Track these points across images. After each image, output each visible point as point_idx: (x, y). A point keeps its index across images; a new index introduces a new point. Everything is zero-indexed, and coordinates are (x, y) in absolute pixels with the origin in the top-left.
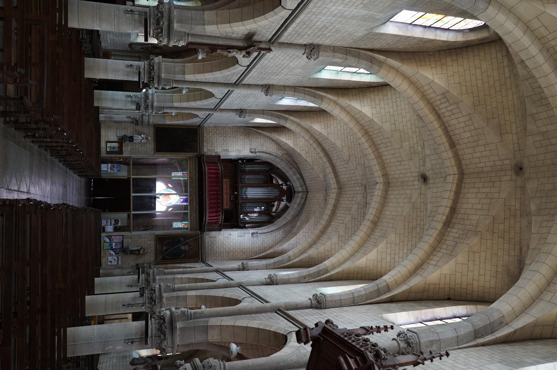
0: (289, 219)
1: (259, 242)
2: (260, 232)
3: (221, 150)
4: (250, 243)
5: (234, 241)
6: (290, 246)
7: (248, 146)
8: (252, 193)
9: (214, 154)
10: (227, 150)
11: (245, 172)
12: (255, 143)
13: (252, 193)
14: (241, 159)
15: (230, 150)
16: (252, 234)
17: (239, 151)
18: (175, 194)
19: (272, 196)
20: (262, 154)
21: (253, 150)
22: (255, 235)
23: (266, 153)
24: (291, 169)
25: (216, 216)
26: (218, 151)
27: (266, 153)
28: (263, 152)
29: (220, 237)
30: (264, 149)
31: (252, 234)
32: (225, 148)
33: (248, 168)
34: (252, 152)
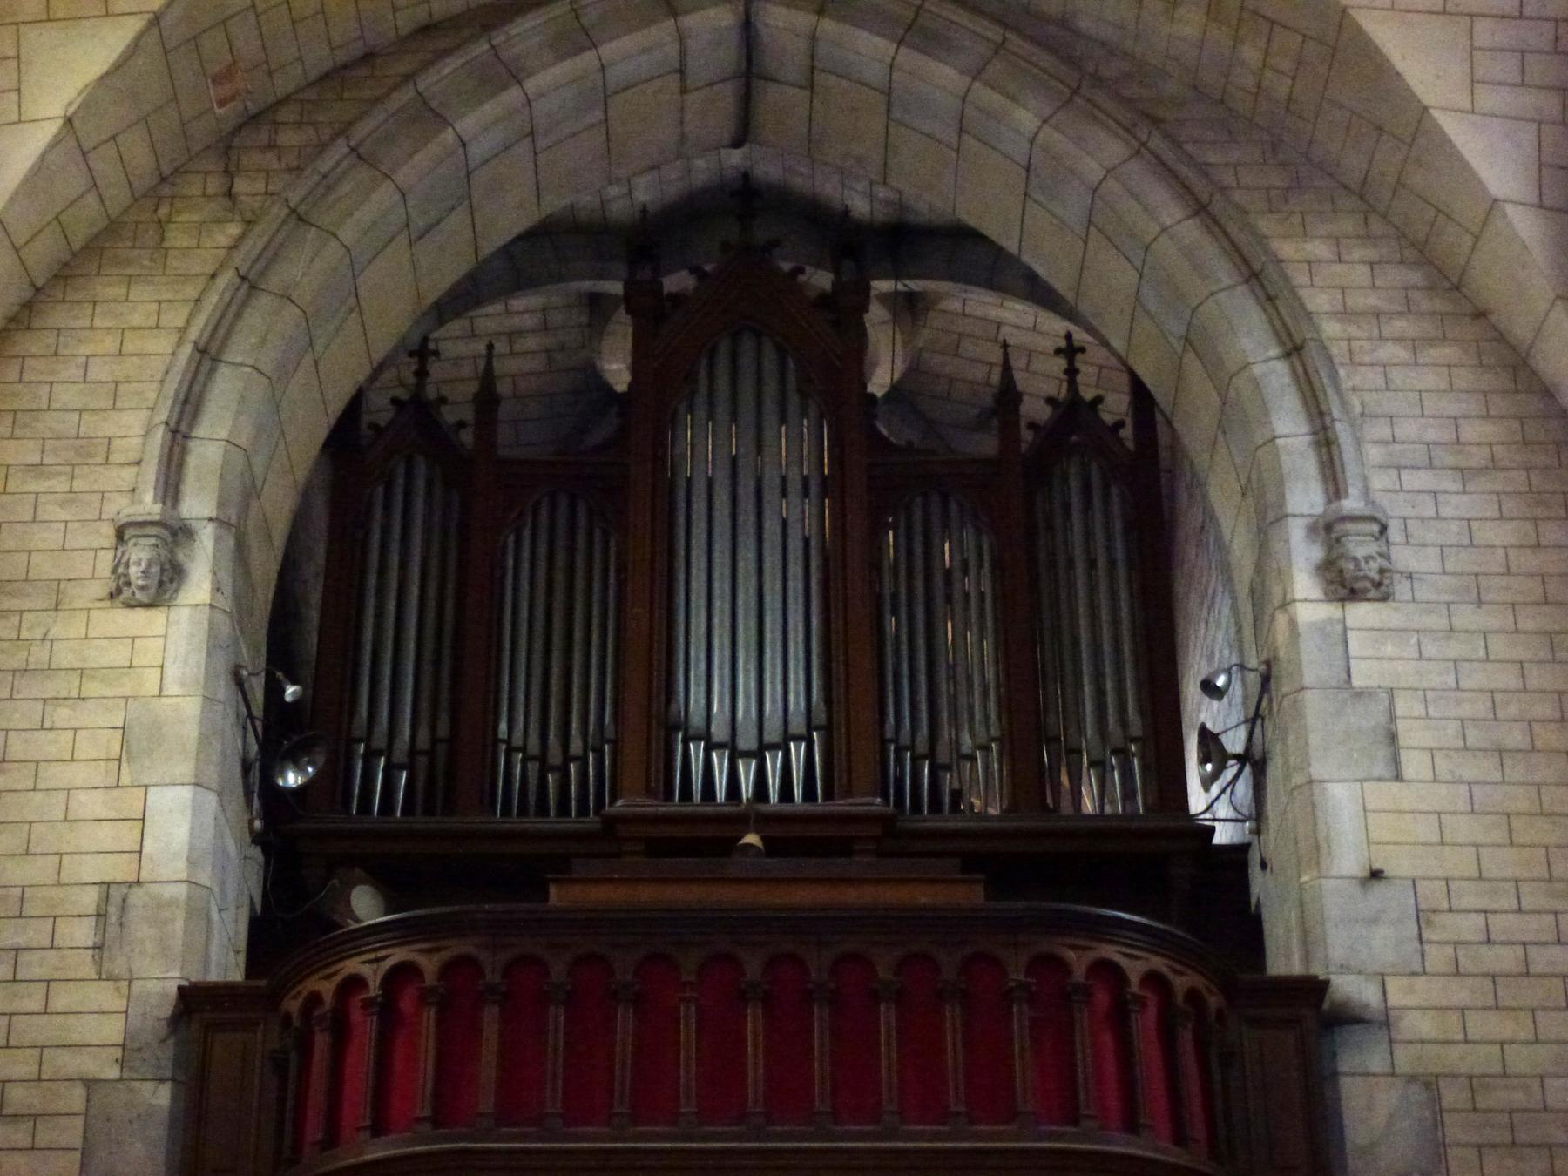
0: (1115, 149)
1: (1456, 505)
2: (1305, 498)
3: (105, 996)
4: (1467, 617)
5: (1464, 828)
6: (1489, 99)
7: (66, 628)
8: (746, 695)
9: (161, 1096)
10: (113, 905)
11: (457, 762)
12: (48, 537)
13: (746, 695)
14: (257, 778)
15: (120, 870)
16: (1344, 585)
17: (133, 743)
18: (1161, 411)
19: (794, 448)
20: (208, 451)
21: (140, 554)
22: (1360, 547)
23: (189, 406)
24: (430, 116)
25: (1120, 1015)
26: (112, 1030)
27: (189, 406)
28: (179, 437)
29: (1418, 1025)
30: (135, 430)
31: (1344, 585)
32: (82, 933)
33: (396, 714)
34: (167, 580)
